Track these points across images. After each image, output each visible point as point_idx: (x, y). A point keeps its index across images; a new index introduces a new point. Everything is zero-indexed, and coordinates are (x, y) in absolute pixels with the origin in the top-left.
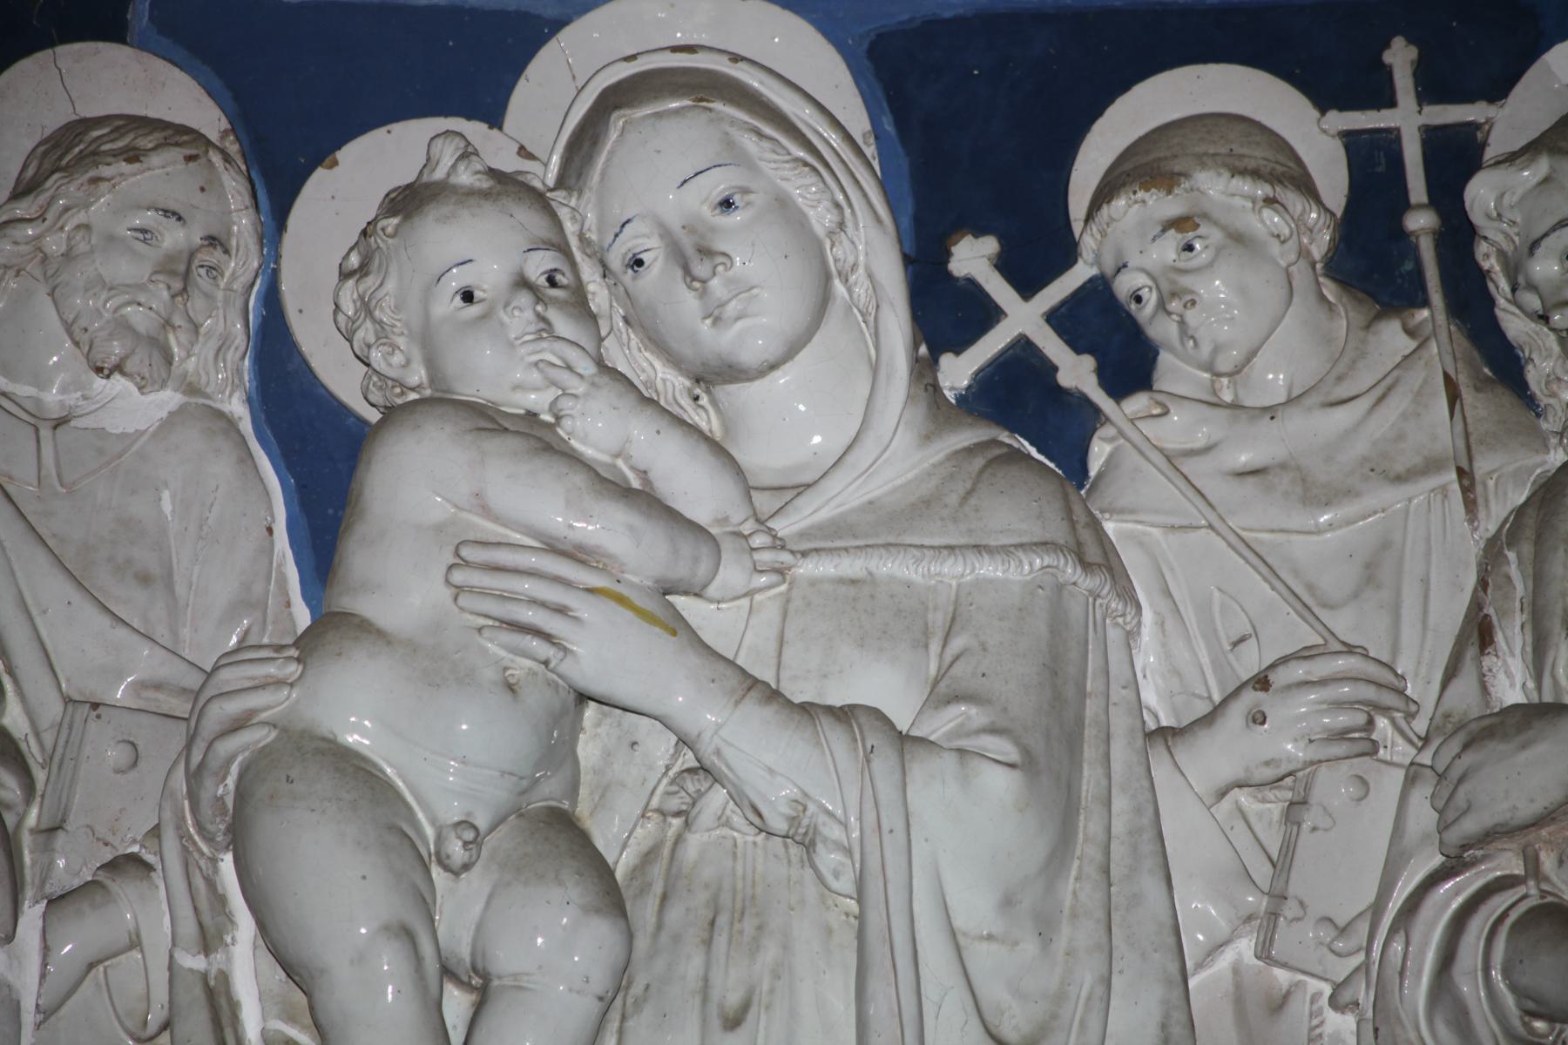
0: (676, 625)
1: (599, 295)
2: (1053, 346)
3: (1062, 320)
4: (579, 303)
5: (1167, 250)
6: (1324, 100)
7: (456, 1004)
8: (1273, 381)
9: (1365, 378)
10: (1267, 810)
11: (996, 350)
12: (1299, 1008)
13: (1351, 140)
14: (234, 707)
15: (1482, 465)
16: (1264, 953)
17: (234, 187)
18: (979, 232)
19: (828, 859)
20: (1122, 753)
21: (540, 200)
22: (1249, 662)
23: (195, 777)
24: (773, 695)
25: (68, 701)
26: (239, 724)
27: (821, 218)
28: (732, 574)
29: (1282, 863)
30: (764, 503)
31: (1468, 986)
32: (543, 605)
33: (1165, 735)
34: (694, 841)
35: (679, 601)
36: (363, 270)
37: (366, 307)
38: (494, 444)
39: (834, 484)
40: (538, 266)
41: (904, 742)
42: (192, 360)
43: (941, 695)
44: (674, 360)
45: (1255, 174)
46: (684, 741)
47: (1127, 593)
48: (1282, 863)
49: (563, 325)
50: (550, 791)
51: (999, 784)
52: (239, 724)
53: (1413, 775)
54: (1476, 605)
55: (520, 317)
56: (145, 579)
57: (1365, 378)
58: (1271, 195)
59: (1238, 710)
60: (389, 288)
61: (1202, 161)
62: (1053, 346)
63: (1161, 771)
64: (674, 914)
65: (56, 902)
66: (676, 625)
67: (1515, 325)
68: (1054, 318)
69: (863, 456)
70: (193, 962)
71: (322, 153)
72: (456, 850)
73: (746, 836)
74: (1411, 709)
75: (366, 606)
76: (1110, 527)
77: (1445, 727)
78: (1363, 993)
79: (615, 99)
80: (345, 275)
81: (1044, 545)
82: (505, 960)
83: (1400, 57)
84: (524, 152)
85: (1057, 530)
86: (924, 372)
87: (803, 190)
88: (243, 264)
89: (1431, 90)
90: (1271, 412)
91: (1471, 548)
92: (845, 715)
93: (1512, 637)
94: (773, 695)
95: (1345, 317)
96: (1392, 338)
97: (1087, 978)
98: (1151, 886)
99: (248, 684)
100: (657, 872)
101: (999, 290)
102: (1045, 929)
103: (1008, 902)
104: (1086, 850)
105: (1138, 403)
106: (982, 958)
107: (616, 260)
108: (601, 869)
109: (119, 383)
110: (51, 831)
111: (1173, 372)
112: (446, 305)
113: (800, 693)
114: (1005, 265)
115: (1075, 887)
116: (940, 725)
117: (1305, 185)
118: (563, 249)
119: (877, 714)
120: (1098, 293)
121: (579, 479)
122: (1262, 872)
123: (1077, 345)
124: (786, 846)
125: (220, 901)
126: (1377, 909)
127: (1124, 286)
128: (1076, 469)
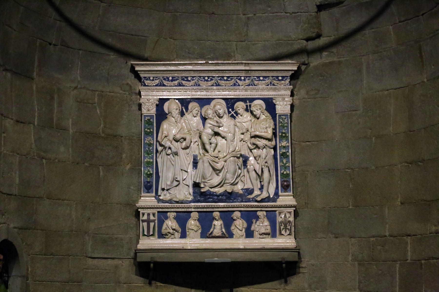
2: (234, 114)
6: (245, 103)
11: (235, 247)
13: (246, 105)
58: (169, 191)
62: (234, 114)
68: (234, 113)
83: (248, 101)
86: (228, 115)
101: (231, 111)
114: (232, 110)
123: (235, 114)
124: (249, 82)
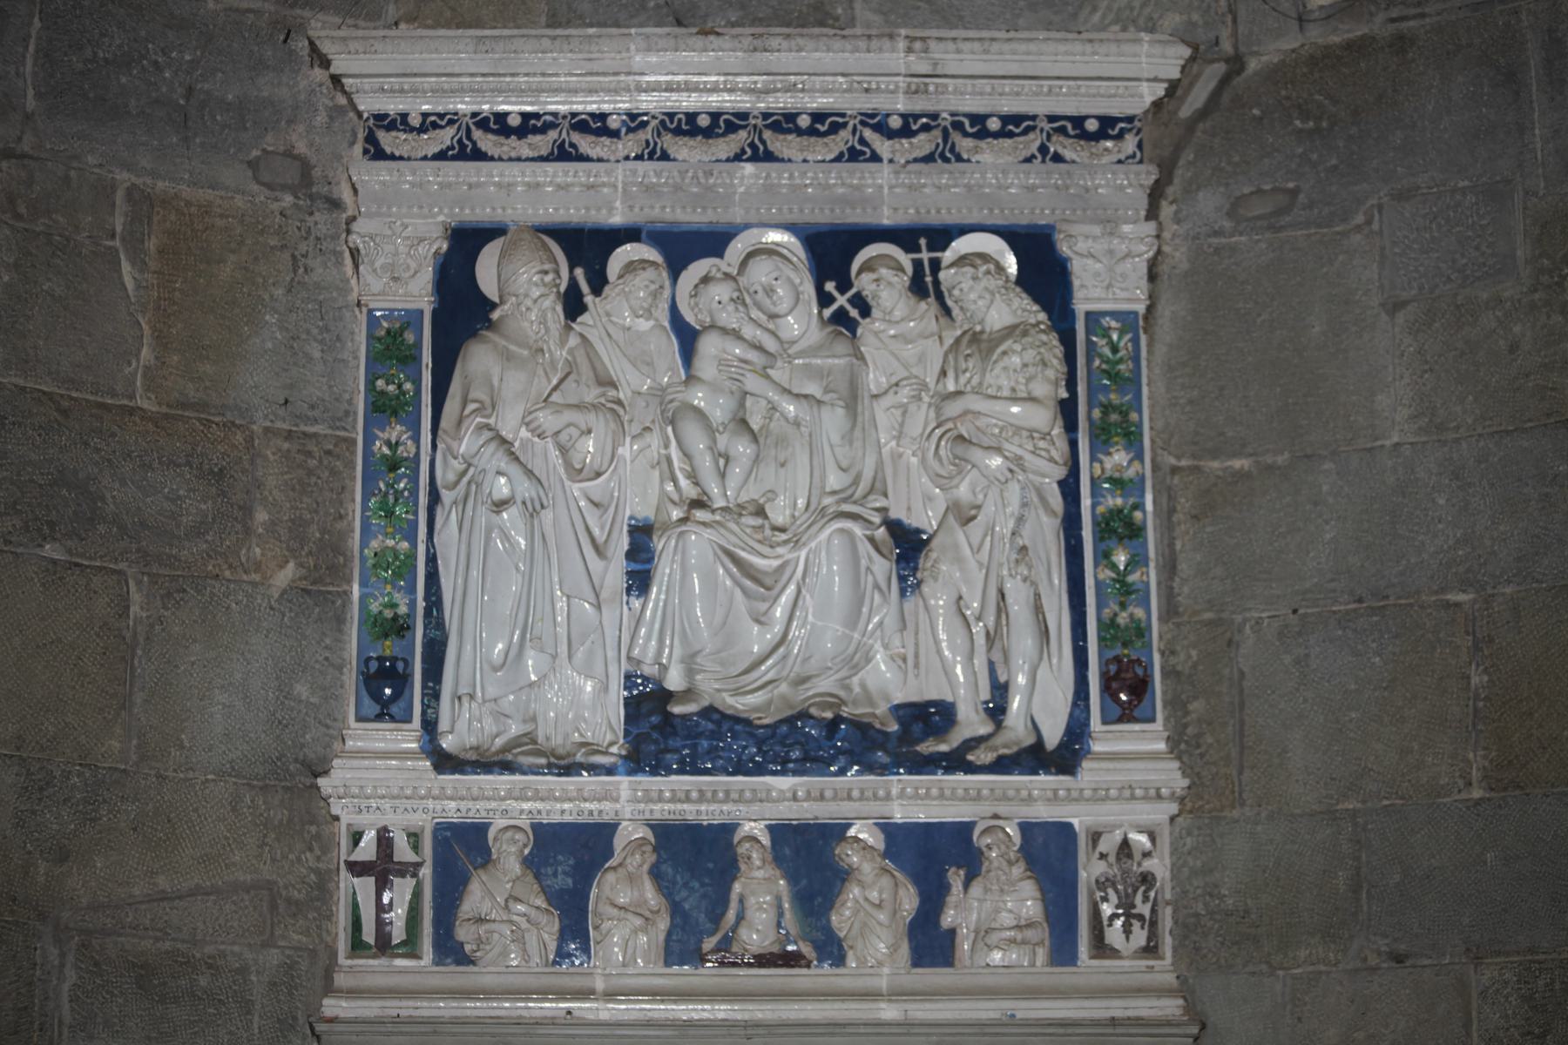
0: (768, 377)
1: (748, 300)
2: (848, 307)
3: (850, 301)
4: (744, 304)
5: (873, 286)
7: (722, 462)
8: (898, 314)
9: (918, 314)
10: (898, 413)
12: (905, 457)
14: (671, 397)
15: (944, 334)
16: (898, 445)
17: (665, 274)
18: (831, 280)
19: (803, 429)
20: (866, 401)
21: (734, 279)
22: (894, 380)
23: (663, 412)
24: (790, 392)
25: (633, 392)
26: (672, 401)
27: (797, 281)
28: (779, 363)
29: (902, 425)
30: (786, 346)
31: (942, 452)
32: (1038, 609)
33: (876, 396)
34: (772, 425)
35: (769, 371)
36: (695, 295)
37: (697, 304)
38: (727, 337)
39: (801, 342)
40: (735, 295)
41: (819, 402)
42: (656, 314)
43: (827, 391)
44: (764, 313)
45: (893, 269)
46: (769, 402)
47: (866, 364)
48: (902, 425)
49: (741, 308)
50: (740, 415)
51: (840, 412)
52: (672, 401)
53: (930, 405)
54: (943, 367)
55: (731, 308)
56: (648, 364)
57: (918, 314)
59: (892, 391)
60: (702, 300)
61: (882, 266)
62: (848, 307)
63: (875, 405)
64: (768, 441)
65: (634, 437)
66: (768, 377)
67: (950, 303)
69: (807, 335)
70: (663, 451)
71: (684, 267)
72: (721, 429)
73: (783, 422)
74: (929, 390)
75: (699, 374)
76: (862, 349)
77: (936, 393)
78: (919, 453)
79: (751, 255)
80: (691, 296)
81: (849, 355)
82: (732, 453)
84: (729, 265)
85: (851, 351)
87: (792, 275)
88: (667, 293)
89: (931, 248)
90: (897, 322)
91: (941, 354)
92: (806, 396)
93: (951, 374)
94: (790, 392)
95: (913, 300)
96: (923, 305)
97: (860, 453)
98: (873, 431)
99: (617, 350)
100: (764, 431)
101: (836, 294)
102: (851, 443)
103: (843, 438)
104: (859, 425)
105: (868, 320)
106: (838, 450)
107: (751, 290)
108: (751, 431)
109: (641, 320)
110: (631, 421)
111: (875, 313)
112: (715, 305)
113: (795, 391)
115: (858, 433)
116: (826, 398)
117: (902, 270)
118: (740, 290)
119: (813, 396)
120: (858, 296)
121: (746, 345)
122: (897, 426)
125: (668, 438)
126: (922, 435)
127: (864, 293)
128: (854, 333)
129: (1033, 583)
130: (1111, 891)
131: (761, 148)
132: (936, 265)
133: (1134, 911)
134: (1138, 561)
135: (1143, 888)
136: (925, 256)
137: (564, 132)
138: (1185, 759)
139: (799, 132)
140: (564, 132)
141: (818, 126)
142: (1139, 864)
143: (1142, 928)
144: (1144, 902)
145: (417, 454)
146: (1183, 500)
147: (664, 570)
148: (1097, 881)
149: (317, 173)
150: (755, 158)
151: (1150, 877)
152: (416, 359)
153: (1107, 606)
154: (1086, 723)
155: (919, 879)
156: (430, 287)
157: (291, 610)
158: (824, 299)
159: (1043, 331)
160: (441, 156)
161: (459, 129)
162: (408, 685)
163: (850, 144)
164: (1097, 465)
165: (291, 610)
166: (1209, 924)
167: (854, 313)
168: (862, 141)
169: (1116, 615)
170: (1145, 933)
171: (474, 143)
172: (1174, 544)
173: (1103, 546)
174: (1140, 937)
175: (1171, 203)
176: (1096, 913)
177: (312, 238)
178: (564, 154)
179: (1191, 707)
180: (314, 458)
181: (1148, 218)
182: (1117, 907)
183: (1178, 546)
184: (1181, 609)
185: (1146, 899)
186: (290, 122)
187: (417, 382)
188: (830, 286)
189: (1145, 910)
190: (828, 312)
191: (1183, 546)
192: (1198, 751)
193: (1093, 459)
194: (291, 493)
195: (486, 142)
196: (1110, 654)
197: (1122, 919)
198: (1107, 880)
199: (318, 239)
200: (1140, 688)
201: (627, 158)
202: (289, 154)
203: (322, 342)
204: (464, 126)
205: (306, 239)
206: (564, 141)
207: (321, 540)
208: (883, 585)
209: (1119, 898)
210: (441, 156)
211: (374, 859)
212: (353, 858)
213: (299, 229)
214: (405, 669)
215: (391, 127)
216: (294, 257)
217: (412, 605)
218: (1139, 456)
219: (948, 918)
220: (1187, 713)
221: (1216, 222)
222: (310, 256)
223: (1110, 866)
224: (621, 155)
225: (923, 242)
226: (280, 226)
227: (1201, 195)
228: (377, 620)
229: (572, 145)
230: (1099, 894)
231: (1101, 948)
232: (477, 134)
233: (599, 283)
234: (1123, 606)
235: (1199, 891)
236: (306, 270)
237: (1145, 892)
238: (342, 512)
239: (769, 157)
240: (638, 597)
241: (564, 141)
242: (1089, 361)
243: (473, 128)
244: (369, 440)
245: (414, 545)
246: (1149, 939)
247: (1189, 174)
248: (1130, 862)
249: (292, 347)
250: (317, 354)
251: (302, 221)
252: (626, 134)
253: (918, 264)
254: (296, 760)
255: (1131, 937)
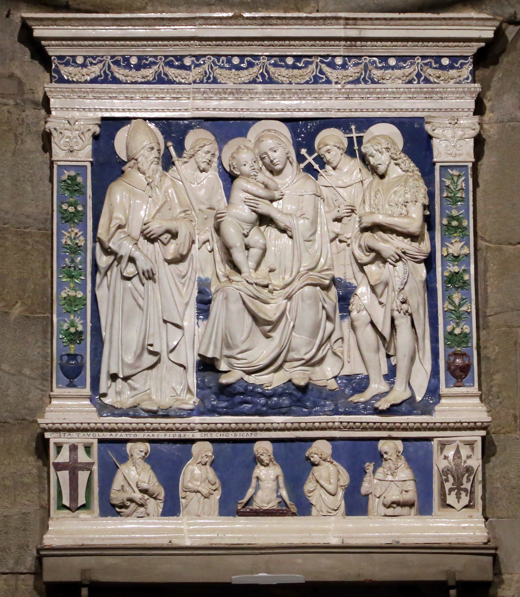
2: (313, 163)
62: (313, 163)
101: (307, 156)
129: (411, 315)
130: (450, 476)
131: (267, 76)
132: (360, 140)
133: (462, 487)
134: (463, 301)
135: (467, 475)
136: (354, 135)
137: (161, 67)
138: (492, 404)
139: (287, 67)
140: (161, 67)
141: (298, 64)
142: (465, 462)
143: (467, 496)
144: (467, 482)
145: (86, 244)
146: (492, 265)
147: (216, 307)
148: (443, 471)
149: (27, 87)
150: (264, 82)
151: (470, 469)
152: (84, 194)
153: (450, 324)
154: (437, 388)
155: (349, 469)
156: (91, 153)
157: (19, 328)
158: (301, 159)
159: (417, 180)
160: (94, 81)
161: (104, 65)
162: (84, 368)
163: (314, 74)
164: (444, 249)
165: (19, 328)
166: (504, 492)
167: (316, 167)
168: (321, 72)
169: (454, 329)
170: (468, 499)
171: (112, 73)
172: (487, 289)
173: (447, 293)
174: (465, 500)
175: (489, 101)
176: (442, 487)
177: (25, 124)
178: (161, 79)
179: (495, 377)
180: (29, 244)
181: (475, 114)
182: (453, 485)
183: (489, 290)
184: (490, 324)
185: (468, 480)
186: (11, 60)
187: (85, 206)
188: (303, 151)
189: (468, 486)
190: (302, 166)
191: (492, 290)
192: (498, 400)
193: (443, 245)
194: (18, 265)
195: (119, 73)
196: (451, 351)
197: (456, 491)
198: (448, 470)
199: (28, 124)
200: (466, 369)
201: (195, 82)
202: (11, 76)
203: (32, 182)
204: (107, 65)
205: (22, 125)
206: (161, 72)
207: (34, 289)
208: (331, 314)
209: (454, 480)
210: (94, 81)
211: (68, 461)
212: (57, 461)
213: (18, 119)
214: (82, 360)
215: (67, 64)
216: (16, 135)
217: (84, 325)
218: (467, 244)
219: (365, 488)
220: (492, 380)
221: (513, 113)
222: (24, 134)
223: (450, 463)
224: (191, 80)
225: (353, 127)
226: (8, 118)
227: (505, 97)
228: (68, 333)
229: (165, 74)
230: (444, 477)
231: (445, 505)
232: (114, 68)
233: (180, 149)
234: (458, 324)
235: (498, 475)
236: (22, 142)
237: (468, 476)
238: (45, 273)
239: (271, 81)
240: (203, 320)
241: (161, 72)
242: (441, 192)
243: (111, 64)
244: (60, 236)
245: (85, 293)
246: (470, 501)
247: (499, 85)
248: (460, 461)
249: (17, 185)
250: (29, 189)
251: (19, 115)
252: (194, 68)
253: (350, 139)
254: (25, 408)
255: (460, 500)
